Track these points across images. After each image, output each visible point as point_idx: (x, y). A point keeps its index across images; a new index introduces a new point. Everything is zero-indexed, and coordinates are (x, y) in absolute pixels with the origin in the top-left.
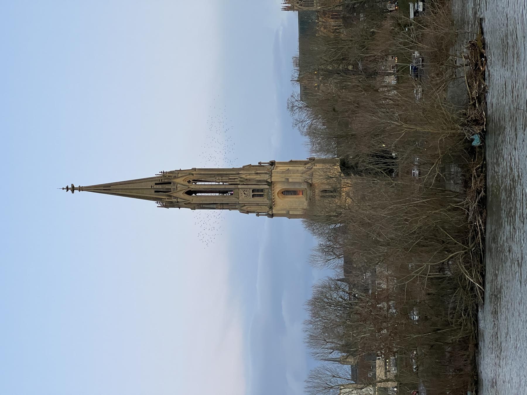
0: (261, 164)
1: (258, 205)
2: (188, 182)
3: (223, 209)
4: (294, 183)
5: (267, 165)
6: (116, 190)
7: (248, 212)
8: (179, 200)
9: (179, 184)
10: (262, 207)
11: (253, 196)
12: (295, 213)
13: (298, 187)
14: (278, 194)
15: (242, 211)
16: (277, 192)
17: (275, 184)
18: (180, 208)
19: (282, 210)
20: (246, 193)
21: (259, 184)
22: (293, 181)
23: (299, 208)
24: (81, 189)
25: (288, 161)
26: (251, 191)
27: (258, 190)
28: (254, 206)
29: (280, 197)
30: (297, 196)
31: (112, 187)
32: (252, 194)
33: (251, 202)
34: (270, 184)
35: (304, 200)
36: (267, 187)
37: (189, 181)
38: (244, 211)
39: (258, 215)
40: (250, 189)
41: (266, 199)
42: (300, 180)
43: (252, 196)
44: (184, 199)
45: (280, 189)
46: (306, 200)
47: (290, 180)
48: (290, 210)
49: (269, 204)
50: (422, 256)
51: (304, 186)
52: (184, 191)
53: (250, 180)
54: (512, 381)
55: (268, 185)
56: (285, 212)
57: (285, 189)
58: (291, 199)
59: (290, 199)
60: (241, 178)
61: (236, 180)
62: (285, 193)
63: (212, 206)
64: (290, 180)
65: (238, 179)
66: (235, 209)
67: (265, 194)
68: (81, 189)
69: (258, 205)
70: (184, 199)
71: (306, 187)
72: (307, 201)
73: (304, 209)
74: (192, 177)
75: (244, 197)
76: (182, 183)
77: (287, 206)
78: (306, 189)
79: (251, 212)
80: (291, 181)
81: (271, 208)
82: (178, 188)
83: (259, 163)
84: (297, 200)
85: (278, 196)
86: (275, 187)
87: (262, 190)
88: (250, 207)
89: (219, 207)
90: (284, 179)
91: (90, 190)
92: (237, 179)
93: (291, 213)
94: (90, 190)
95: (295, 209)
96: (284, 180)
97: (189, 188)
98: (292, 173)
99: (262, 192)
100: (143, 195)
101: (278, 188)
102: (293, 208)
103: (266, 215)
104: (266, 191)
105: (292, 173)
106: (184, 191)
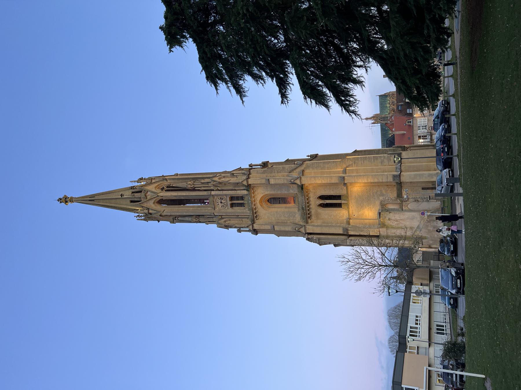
0: (252, 166)
1: (237, 217)
2: (161, 189)
3: (200, 222)
4: (280, 186)
5: (259, 167)
6: (98, 201)
7: (227, 227)
8: (150, 211)
9: (150, 191)
10: (243, 219)
11: (232, 205)
12: (283, 228)
13: (286, 192)
14: (261, 201)
15: (220, 226)
16: (259, 199)
17: (255, 189)
18: (159, 222)
19: (266, 224)
20: (223, 201)
21: (236, 189)
22: (275, 182)
23: (289, 222)
24: (72, 200)
25: (283, 160)
26: (228, 199)
27: (238, 198)
28: (233, 219)
29: (264, 206)
30: (288, 205)
31: (96, 198)
32: (230, 202)
33: (230, 213)
34: (249, 187)
35: (296, 210)
36: (245, 192)
37: (163, 187)
38: (221, 226)
39: (239, 231)
40: (226, 195)
41: (247, 209)
42: (285, 181)
43: (229, 206)
44: (155, 210)
45: (262, 195)
46: (299, 210)
47: (272, 181)
48: (276, 225)
49: (250, 216)
50: (367, 240)
51: (294, 190)
52: (154, 199)
53: (225, 184)
54: (393, 228)
55: (247, 190)
56: (268, 227)
57: (271, 195)
58: (279, 210)
59: (278, 209)
60: (215, 181)
61: (210, 185)
62: (273, 200)
63: (187, 219)
64: (272, 181)
65: (212, 183)
66: (213, 222)
67: (246, 202)
68: (72, 200)
69: (237, 217)
70: (155, 210)
71: (296, 192)
72: (300, 212)
73: (294, 224)
74: (166, 184)
75: (221, 206)
76: (154, 190)
77: (273, 219)
78: (297, 193)
79: (231, 227)
80: (273, 183)
81: (253, 222)
82: (148, 197)
83: (250, 166)
84: (286, 210)
85: (261, 206)
86: (256, 193)
87: (242, 198)
88: (230, 220)
89: (194, 220)
90: (264, 180)
91: (80, 201)
92: (210, 182)
93: (277, 228)
94: (80, 201)
95: (284, 223)
96: (264, 181)
97: (158, 196)
98: (276, 172)
99: (243, 200)
100: (120, 206)
101: (260, 194)
102: (280, 221)
103: (249, 231)
104: (246, 198)
105: (276, 172)
106: (154, 199)
